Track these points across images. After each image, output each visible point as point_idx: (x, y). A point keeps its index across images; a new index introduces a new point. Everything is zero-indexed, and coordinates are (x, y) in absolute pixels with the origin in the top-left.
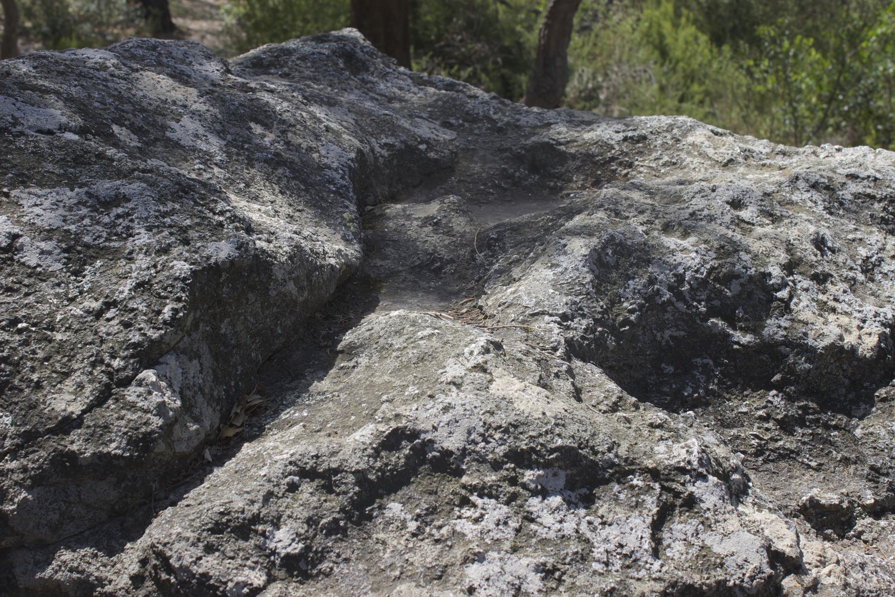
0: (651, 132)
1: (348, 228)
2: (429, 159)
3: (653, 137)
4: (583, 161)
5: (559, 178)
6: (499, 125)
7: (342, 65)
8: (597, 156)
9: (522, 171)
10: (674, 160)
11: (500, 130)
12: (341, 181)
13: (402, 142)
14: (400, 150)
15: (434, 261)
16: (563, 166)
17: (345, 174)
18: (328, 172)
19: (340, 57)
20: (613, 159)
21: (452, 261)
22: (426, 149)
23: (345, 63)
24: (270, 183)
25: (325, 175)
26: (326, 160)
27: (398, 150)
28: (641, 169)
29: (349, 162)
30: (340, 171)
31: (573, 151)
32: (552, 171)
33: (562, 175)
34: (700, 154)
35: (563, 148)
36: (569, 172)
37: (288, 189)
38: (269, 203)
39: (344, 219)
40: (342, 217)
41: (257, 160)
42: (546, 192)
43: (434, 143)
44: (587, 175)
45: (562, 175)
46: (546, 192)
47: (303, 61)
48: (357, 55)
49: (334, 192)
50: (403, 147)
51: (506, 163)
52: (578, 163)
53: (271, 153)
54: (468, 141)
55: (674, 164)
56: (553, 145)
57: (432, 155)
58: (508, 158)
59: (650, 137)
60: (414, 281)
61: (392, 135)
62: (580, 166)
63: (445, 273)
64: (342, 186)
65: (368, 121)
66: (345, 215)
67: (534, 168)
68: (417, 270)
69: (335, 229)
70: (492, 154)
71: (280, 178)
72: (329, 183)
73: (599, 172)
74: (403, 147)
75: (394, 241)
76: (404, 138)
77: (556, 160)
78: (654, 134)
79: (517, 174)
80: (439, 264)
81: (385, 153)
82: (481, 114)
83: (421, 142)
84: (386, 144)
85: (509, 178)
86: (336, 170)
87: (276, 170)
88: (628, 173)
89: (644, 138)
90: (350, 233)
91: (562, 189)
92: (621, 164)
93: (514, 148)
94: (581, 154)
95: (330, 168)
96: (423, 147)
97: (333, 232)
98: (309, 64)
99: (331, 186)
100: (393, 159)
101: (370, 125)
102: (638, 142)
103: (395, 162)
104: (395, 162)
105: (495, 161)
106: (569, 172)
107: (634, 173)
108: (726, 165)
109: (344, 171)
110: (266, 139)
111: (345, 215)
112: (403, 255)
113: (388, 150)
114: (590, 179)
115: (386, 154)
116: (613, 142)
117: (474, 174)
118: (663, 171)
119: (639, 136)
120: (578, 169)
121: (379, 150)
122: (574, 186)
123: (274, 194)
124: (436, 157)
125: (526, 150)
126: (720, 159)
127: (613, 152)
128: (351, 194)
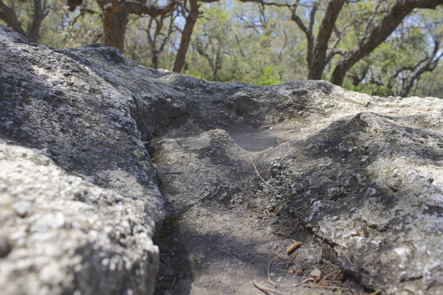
0: (309, 89)
1: (141, 167)
2: (174, 107)
3: (311, 91)
4: (269, 107)
5: (256, 118)
6: (208, 89)
7: (109, 58)
8: (278, 103)
9: (232, 115)
10: (331, 104)
11: (209, 92)
12: (125, 118)
13: (156, 96)
14: (155, 101)
15: (220, 191)
16: (257, 110)
17: (127, 112)
18: (112, 111)
19: (108, 54)
20: (289, 105)
21: (238, 190)
22: (171, 102)
23: (110, 57)
24: (49, 120)
25: (109, 113)
26: (108, 101)
27: (154, 102)
28: (312, 110)
29: (129, 103)
30: (123, 110)
31: (262, 101)
32: (251, 114)
33: (257, 116)
34: (166, 126)
35: (255, 99)
36: (262, 114)
37: (71, 127)
38: (46, 144)
39: (134, 157)
40: (133, 155)
41: (35, 97)
42: (251, 127)
43: (175, 98)
44: (274, 115)
45: (257, 116)
46: (251, 127)
47: (85, 53)
48: (117, 54)
49: (119, 129)
50: (157, 99)
51: (222, 110)
52: (267, 108)
53: (52, 91)
54: (193, 97)
55: (332, 106)
56: (249, 98)
57: (175, 105)
58: (222, 106)
59: (309, 91)
60: (208, 215)
61: (149, 92)
62: (268, 110)
63: (234, 203)
64: (127, 123)
65: (132, 82)
66: (135, 152)
67: (239, 112)
68: (207, 202)
69: (127, 170)
70: (210, 105)
71: (61, 116)
72: (115, 120)
73: (282, 114)
74: (157, 99)
75: (178, 173)
76: (157, 94)
77: (252, 107)
78: (311, 90)
79: (231, 116)
80: (225, 194)
81: (146, 102)
82: (195, 83)
83: (168, 97)
84: (146, 98)
85: (226, 119)
86: (119, 109)
87: (58, 107)
88: (303, 113)
89: (305, 92)
90: (144, 173)
91: (260, 125)
92: (295, 108)
93: (225, 101)
94: (267, 103)
95: (113, 107)
96: (169, 100)
97: (126, 174)
98: (89, 56)
99: (117, 124)
100: (151, 107)
101: (134, 85)
102: (302, 94)
103: (153, 109)
104: (153, 109)
105: (214, 109)
106: (262, 114)
107: (308, 113)
108: (367, 106)
109: (126, 110)
110: (49, 80)
111: (135, 152)
112: (191, 187)
113: (148, 101)
114: (276, 118)
115: (147, 104)
116: (287, 95)
117: (203, 117)
118: (326, 111)
119: (302, 91)
120: (267, 112)
121: (143, 101)
122: (268, 122)
123: (53, 133)
124: (178, 106)
125: (233, 101)
126: (362, 103)
127: (289, 100)
128: (136, 131)
